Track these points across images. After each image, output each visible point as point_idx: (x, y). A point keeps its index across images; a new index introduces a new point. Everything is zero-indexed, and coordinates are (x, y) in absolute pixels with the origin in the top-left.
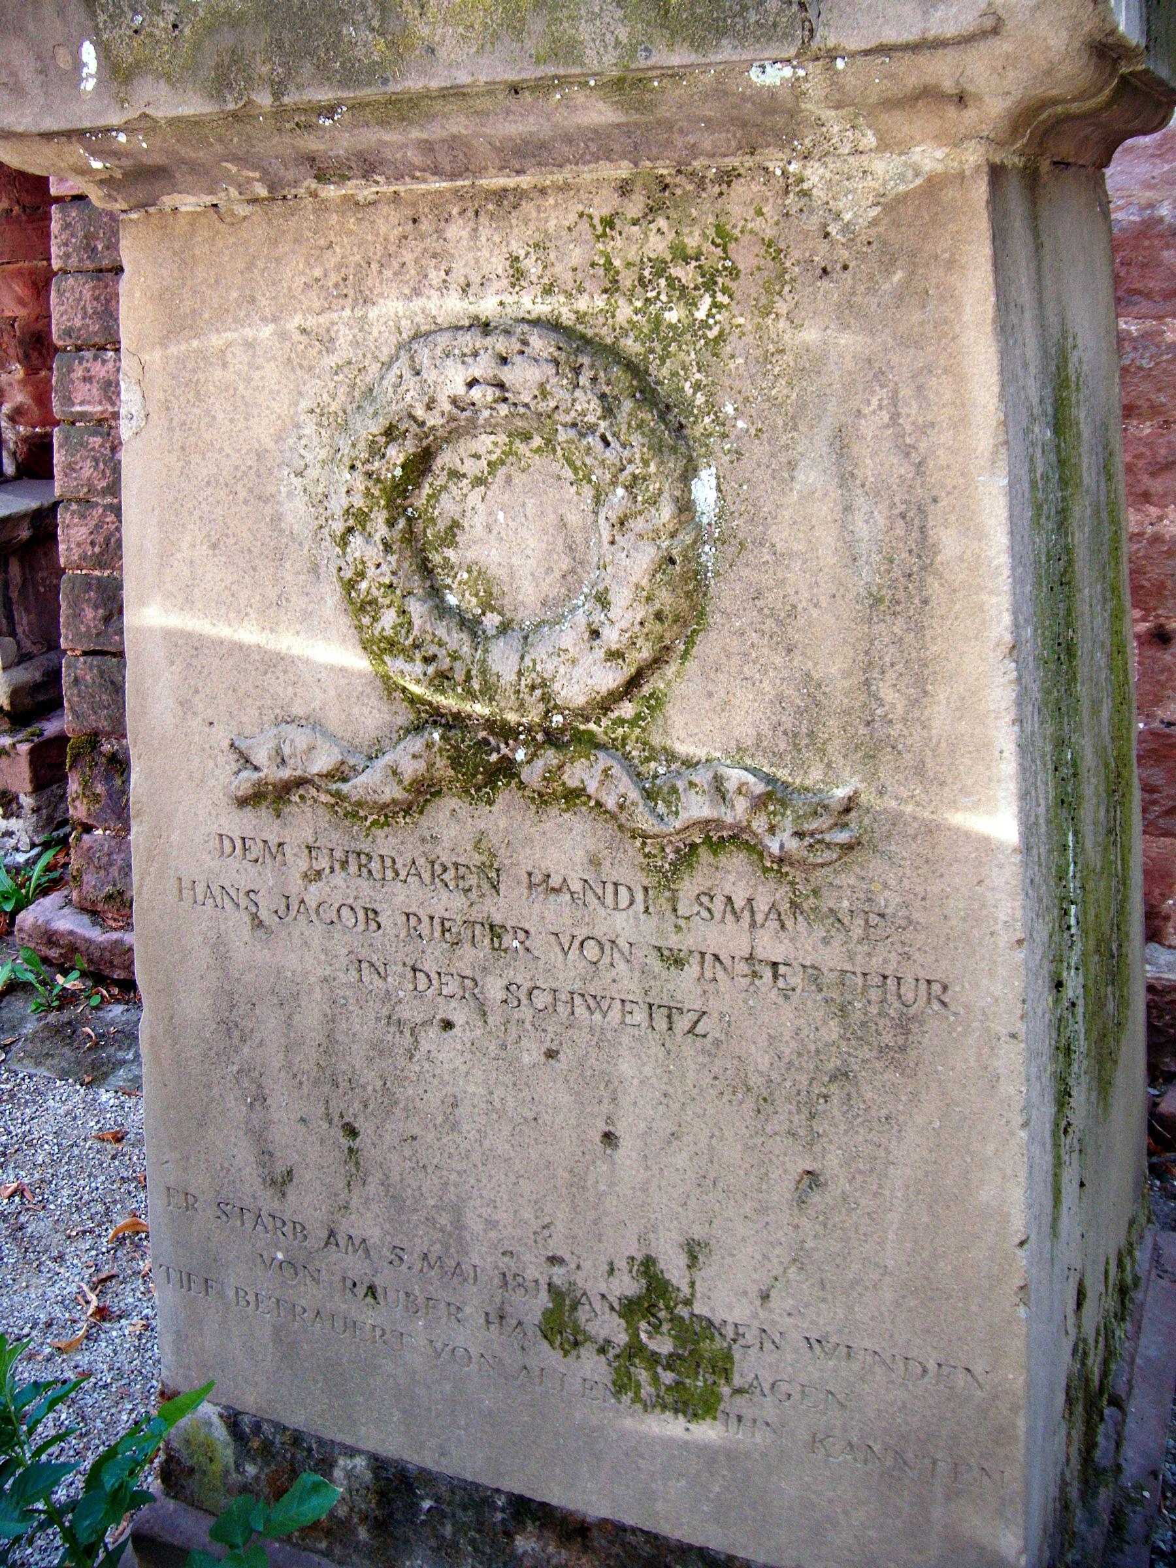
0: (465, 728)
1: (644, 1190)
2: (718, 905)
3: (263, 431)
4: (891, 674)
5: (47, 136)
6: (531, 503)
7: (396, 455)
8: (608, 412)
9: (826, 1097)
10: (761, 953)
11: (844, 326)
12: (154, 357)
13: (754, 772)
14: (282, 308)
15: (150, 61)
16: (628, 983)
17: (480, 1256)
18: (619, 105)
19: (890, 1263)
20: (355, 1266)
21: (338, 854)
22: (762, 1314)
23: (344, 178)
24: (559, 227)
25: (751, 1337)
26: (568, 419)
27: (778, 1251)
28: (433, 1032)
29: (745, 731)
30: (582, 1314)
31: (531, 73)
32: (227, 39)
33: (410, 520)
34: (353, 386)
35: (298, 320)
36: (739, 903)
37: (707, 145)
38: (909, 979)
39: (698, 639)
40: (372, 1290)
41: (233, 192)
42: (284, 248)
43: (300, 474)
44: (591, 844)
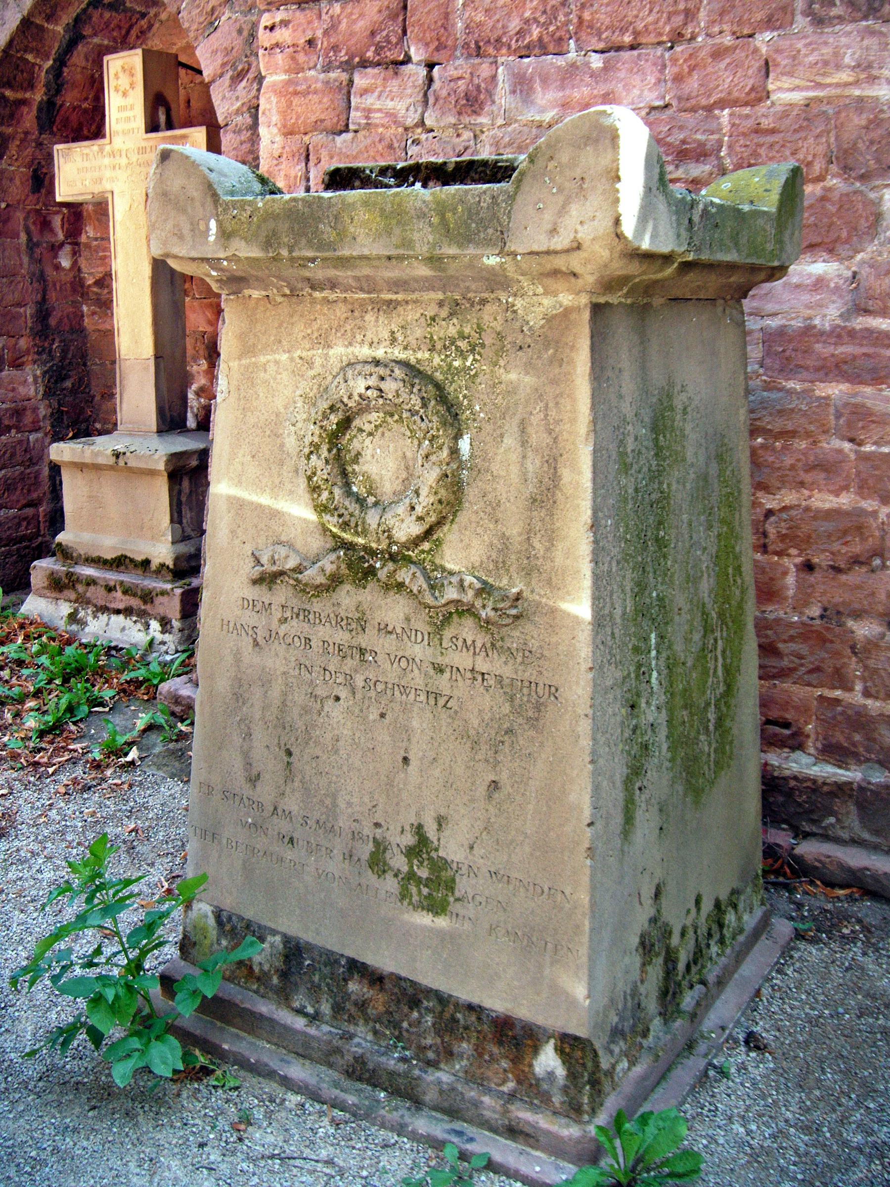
0: (354, 550)
1: (420, 788)
2: (460, 643)
3: (279, 404)
4: (539, 535)
5: (193, 259)
6: (391, 445)
7: (334, 419)
8: (424, 405)
9: (503, 742)
10: (477, 668)
11: (527, 373)
12: (234, 364)
13: (478, 578)
14: (292, 346)
15: (238, 231)
16: (417, 679)
17: (343, 823)
18: (432, 268)
19: (529, 832)
20: (284, 826)
21: (295, 610)
22: (470, 857)
23: (323, 289)
24: (412, 319)
25: (464, 870)
26: (407, 407)
27: (478, 823)
28: (331, 702)
29: (475, 559)
30: (388, 855)
31: (393, 252)
32: (271, 224)
33: (339, 450)
34: (320, 385)
35: (299, 353)
36: (469, 643)
37: (473, 287)
38: (541, 685)
39: (459, 514)
40: (291, 840)
41: (275, 291)
42: (295, 318)
43: (294, 425)
44: (406, 610)
